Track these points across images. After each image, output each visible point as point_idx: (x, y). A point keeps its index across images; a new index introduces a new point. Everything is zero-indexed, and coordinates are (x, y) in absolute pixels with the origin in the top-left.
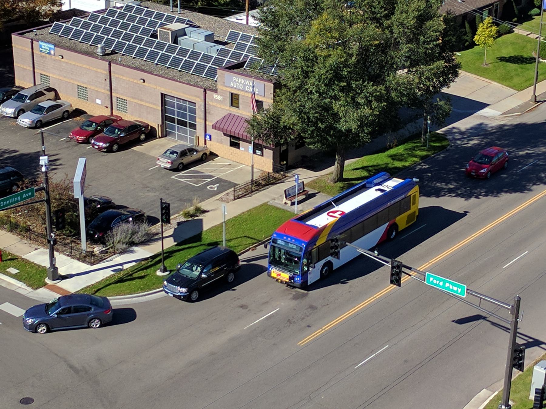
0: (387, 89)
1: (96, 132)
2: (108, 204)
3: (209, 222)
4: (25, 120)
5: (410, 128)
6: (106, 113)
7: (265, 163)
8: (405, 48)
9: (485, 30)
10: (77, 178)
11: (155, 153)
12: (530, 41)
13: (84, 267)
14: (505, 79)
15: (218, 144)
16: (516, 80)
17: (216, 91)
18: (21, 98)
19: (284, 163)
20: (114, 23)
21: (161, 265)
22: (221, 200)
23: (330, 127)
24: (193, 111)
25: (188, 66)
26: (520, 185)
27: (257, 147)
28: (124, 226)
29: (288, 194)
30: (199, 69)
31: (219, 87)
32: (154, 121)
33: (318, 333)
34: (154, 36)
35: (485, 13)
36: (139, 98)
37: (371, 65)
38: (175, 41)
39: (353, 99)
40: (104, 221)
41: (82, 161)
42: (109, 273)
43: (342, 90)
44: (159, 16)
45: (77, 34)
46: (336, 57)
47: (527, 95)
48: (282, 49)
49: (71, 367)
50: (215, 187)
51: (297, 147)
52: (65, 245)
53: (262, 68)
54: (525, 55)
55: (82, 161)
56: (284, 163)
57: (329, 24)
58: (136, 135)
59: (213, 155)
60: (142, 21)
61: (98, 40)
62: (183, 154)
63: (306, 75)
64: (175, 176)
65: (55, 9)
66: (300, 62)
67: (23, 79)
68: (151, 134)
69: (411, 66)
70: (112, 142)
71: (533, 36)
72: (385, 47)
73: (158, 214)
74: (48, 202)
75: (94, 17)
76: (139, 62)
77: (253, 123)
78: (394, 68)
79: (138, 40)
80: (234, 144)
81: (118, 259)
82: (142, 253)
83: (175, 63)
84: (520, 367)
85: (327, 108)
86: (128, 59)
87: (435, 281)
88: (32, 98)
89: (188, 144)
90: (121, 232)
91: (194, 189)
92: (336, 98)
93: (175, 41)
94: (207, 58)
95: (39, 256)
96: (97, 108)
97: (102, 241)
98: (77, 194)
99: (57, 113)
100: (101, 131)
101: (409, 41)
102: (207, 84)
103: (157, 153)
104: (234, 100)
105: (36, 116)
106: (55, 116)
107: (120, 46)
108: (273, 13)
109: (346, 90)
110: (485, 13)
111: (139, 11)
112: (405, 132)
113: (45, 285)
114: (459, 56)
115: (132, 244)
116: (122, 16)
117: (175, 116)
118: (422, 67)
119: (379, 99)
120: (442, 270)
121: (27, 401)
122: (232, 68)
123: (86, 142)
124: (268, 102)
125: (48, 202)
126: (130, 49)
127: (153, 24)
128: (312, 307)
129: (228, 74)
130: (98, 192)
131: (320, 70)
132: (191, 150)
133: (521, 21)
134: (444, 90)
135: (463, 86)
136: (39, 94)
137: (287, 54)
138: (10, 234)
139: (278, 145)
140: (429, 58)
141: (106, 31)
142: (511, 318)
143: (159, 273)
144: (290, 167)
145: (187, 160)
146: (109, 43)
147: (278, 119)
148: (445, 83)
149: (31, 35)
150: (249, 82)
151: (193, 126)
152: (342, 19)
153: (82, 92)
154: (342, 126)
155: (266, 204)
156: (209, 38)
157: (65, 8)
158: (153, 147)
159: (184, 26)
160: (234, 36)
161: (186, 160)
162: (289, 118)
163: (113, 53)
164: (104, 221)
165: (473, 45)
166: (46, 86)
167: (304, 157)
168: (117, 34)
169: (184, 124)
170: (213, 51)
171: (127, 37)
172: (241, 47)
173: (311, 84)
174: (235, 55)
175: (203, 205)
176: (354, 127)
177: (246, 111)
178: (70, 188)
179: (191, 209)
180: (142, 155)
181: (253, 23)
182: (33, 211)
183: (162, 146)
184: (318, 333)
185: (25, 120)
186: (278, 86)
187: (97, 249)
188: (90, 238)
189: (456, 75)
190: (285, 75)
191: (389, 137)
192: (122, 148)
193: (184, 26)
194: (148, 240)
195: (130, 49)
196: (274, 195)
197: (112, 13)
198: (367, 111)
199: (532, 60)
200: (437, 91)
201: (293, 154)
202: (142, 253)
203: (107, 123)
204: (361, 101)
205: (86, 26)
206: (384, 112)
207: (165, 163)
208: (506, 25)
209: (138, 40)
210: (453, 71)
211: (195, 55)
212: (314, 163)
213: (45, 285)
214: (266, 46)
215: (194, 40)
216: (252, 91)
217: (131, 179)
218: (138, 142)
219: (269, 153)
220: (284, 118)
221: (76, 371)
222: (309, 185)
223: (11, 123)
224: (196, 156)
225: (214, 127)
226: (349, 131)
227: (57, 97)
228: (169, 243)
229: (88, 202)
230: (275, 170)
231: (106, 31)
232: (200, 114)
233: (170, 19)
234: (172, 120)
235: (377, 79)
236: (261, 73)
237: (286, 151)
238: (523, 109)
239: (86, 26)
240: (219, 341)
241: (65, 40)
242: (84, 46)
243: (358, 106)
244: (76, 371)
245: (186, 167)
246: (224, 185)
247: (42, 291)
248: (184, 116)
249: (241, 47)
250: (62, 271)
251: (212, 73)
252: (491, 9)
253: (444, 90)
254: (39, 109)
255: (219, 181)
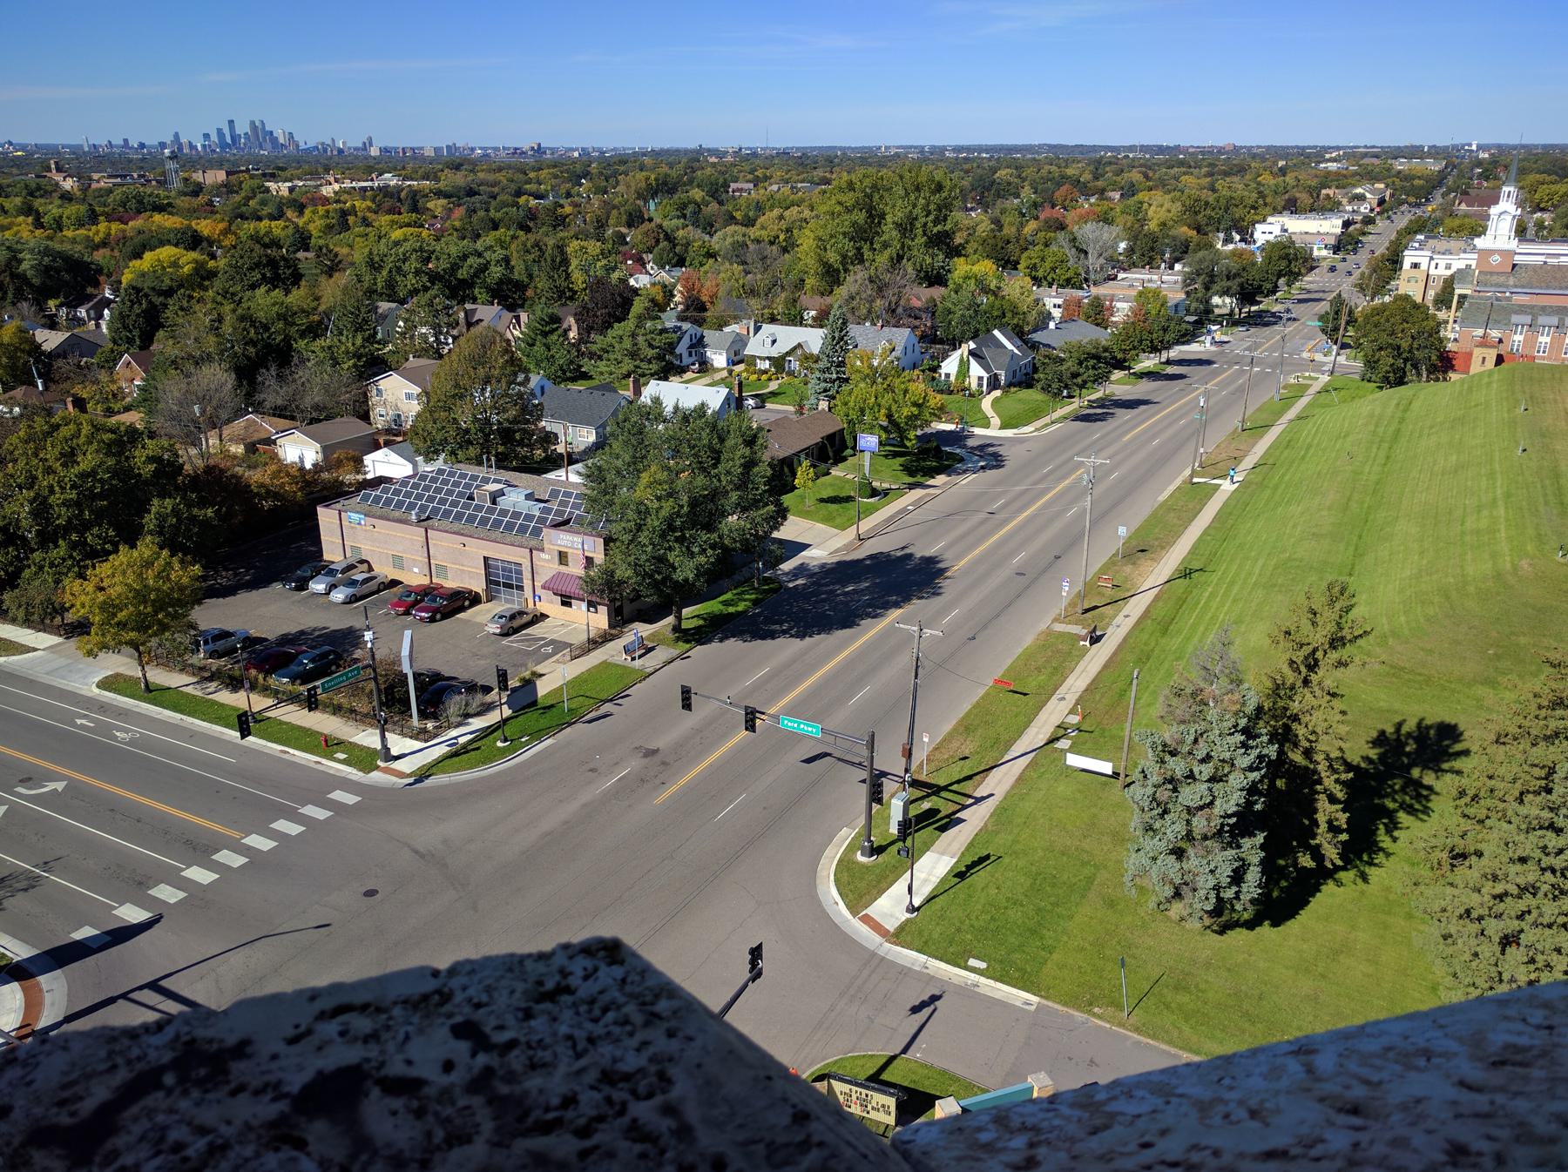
0: (720, 537)
1: (416, 602)
2: (437, 677)
3: (543, 688)
4: (338, 596)
5: (745, 572)
6: (426, 581)
7: (600, 620)
8: (734, 496)
9: (804, 472)
10: (405, 652)
11: (479, 619)
12: (848, 481)
13: (418, 745)
14: (828, 520)
15: (549, 604)
16: (838, 520)
17: (542, 550)
18: (332, 573)
19: (620, 618)
20: (427, 488)
21: (499, 733)
22: (557, 661)
23: (667, 578)
24: (520, 573)
25: (509, 527)
26: (847, 619)
27: (591, 604)
28: (457, 698)
29: (627, 650)
30: (523, 529)
31: (546, 546)
32: (479, 586)
33: (673, 789)
34: (471, 498)
35: (803, 456)
36: (459, 561)
37: (704, 513)
38: (494, 502)
39: (688, 548)
40: (436, 695)
41: (408, 633)
42: (443, 750)
43: (677, 540)
44: (474, 478)
45: (388, 502)
46: (668, 507)
47: (851, 534)
48: (611, 503)
49: (417, 852)
50: (550, 649)
51: (632, 601)
52: (395, 723)
53: (591, 523)
54: (843, 494)
55: (408, 633)
56: (620, 618)
57: (658, 476)
58: (461, 601)
59: (544, 616)
60: (456, 484)
61: (411, 506)
62: (513, 617)
63: (639, 528)
64: (505, 641)
65: (360, 477)
66: (631, 514)
67: (332, 552)
68: (475, 600)
69: (744, 510)
70: (435, 611)
71: (850, 477)
72: (715, 495)
73: (493, 681)
74: (375, 679)
75: (404, 482)
76: (457, 526)
77: (589, 581)
78: (724, 514)
79: (454, 504)
80: (566, 603)
81: (454, 733)
82: (478, 723)
83: (497, 524)
84: (880, 801)
85: (662, 560)
86: (445, 524)
87: (789, 724)
88: (344, 571)
89: (516, 607)
90: (454, 705)
91: (528, 654)
92: (670, 549)
93: (494, 502)
94: (529, 517)
95: (369, 738)
96: (415, 577)
97: (435, 717)
98: (406, 668)
99: (373, 585)
100: (422, 600)
101: (737, 489)
102: (533, 543)
103: (485, 617)
104: (563, 558)
105: (350, 591)
106: (369, 589)
107: (435, 511)
108: (600, 469)
109: (678, 540)
110: (803, 456)
111: (452, 474)
112: (737, 577)
113: (377, 767)
114: (787, 499)
115: (467, 716)
116: (434, 480)
117: (500, 579)
118: (752, 514)
119: (713, 547)
120: (794, 711)
121: (371, 893)
122: (557, 526)
123: (407, 613)
124: (599, 557)
125: (375, 679)
126: (447, 514)
127: (468, 486)
128: (664, 763)
129: (553, 532)
130: (428, 664)
131: (654, 522)
132: (521, 613)
133: (836, 463)
134: (775, 535)
135: (790, 530)
136: (351, 567)
137: (617, 508)
138: (333, 718)
139: (612, 601)
140: (756, 503)
141: (419, 497)
142: (866, 753)
143: (499, 744)
144: (627, 621)
145: (517, 623)
146: (423, 509)
147: (612, 573)
148: (776, 527)
149: (338, 506)
150: (578, 539)
151: (521, 588)
152: (669, 469)
153: (398, 562)
154: (679, 576)
155: (605, 662)
156: (529, 497)
157: (369, 476)
158: (477, 613)
159: (501, 486)
160: (555, 494)
161: (516, 623)
162: (623, 572)
163: (428, 518)
164: (436, 695)
165: (794, 488)
166: (358, 557)
167: (639, 611)
168: (431, 499)
169: (510, 586)
170: (536, 509)
171: (443, 502)
172: (563, 504)
173: (643, 538)
174: (559, 513)
175: (540, 669)
176: (691, 576)
177: (576, 569)
178: (397, 661)
179: (527, 674)
180: (466, 622)
181: (574, 478)
182: (355, 690)
183: (489, 611)
184: (673, 789)
185: (338, 596)
186: (608, 541)
187: (430, 725)
188: (423, 715)
189: (785, 518)
190: (615, 528)
191: (726, 583)
192: (444, 617)
193: (501, 486)
194: (486, 708)
195: (447, 514)
196: (613, 652)
197: (423, 478)
198: (703, 559)
199: (849, 499)
200: (767, 535)
201: (627, 610)
202: (478, 723)
203: (427, 592)
204: (696, 550)
205: (397, 492)
206: (719, 559)
207: (494, 628)
208: (823, 466)
209: (454, 504)
210: (782, 514)
211: (516, 515)
212: (650, 616)
213: (377, 767)
214: (593, 500)
215: (515, 499)
216: (581, 548)
217: (466, 646)
218: (463, 609)
219: (603, 610)
220: (618, 573)
221: (422, 856)
222: (648, 638)
223: (322, 600)
224: (526, 619)
225: (544, 587)
226: (686, 580)
227: (371, 569)
228: (507, 712)
229: (416, 676)
230: (611, 626)
231: (419, 497)
232: (527, 575)
233: (486, 481)
234: (498, 583)
235: (709, 527)
236: (590, 528)
237: (621, 607)
238: (848, 547)
239: (397, 492)
240: (573, 807)
241: (376, 509)
242: (397, 514)
243: (692, 555)
244: (422, 856)
245: (516, 631)
246: (559, 646)
247: (375, 775)
248: (510, 578)
249: (563, 504)
250: (394, 752)
251: (537, 532)
252: (808, 452)
253: (775, 535)
254: (353, 583)
255: (553, 642)
